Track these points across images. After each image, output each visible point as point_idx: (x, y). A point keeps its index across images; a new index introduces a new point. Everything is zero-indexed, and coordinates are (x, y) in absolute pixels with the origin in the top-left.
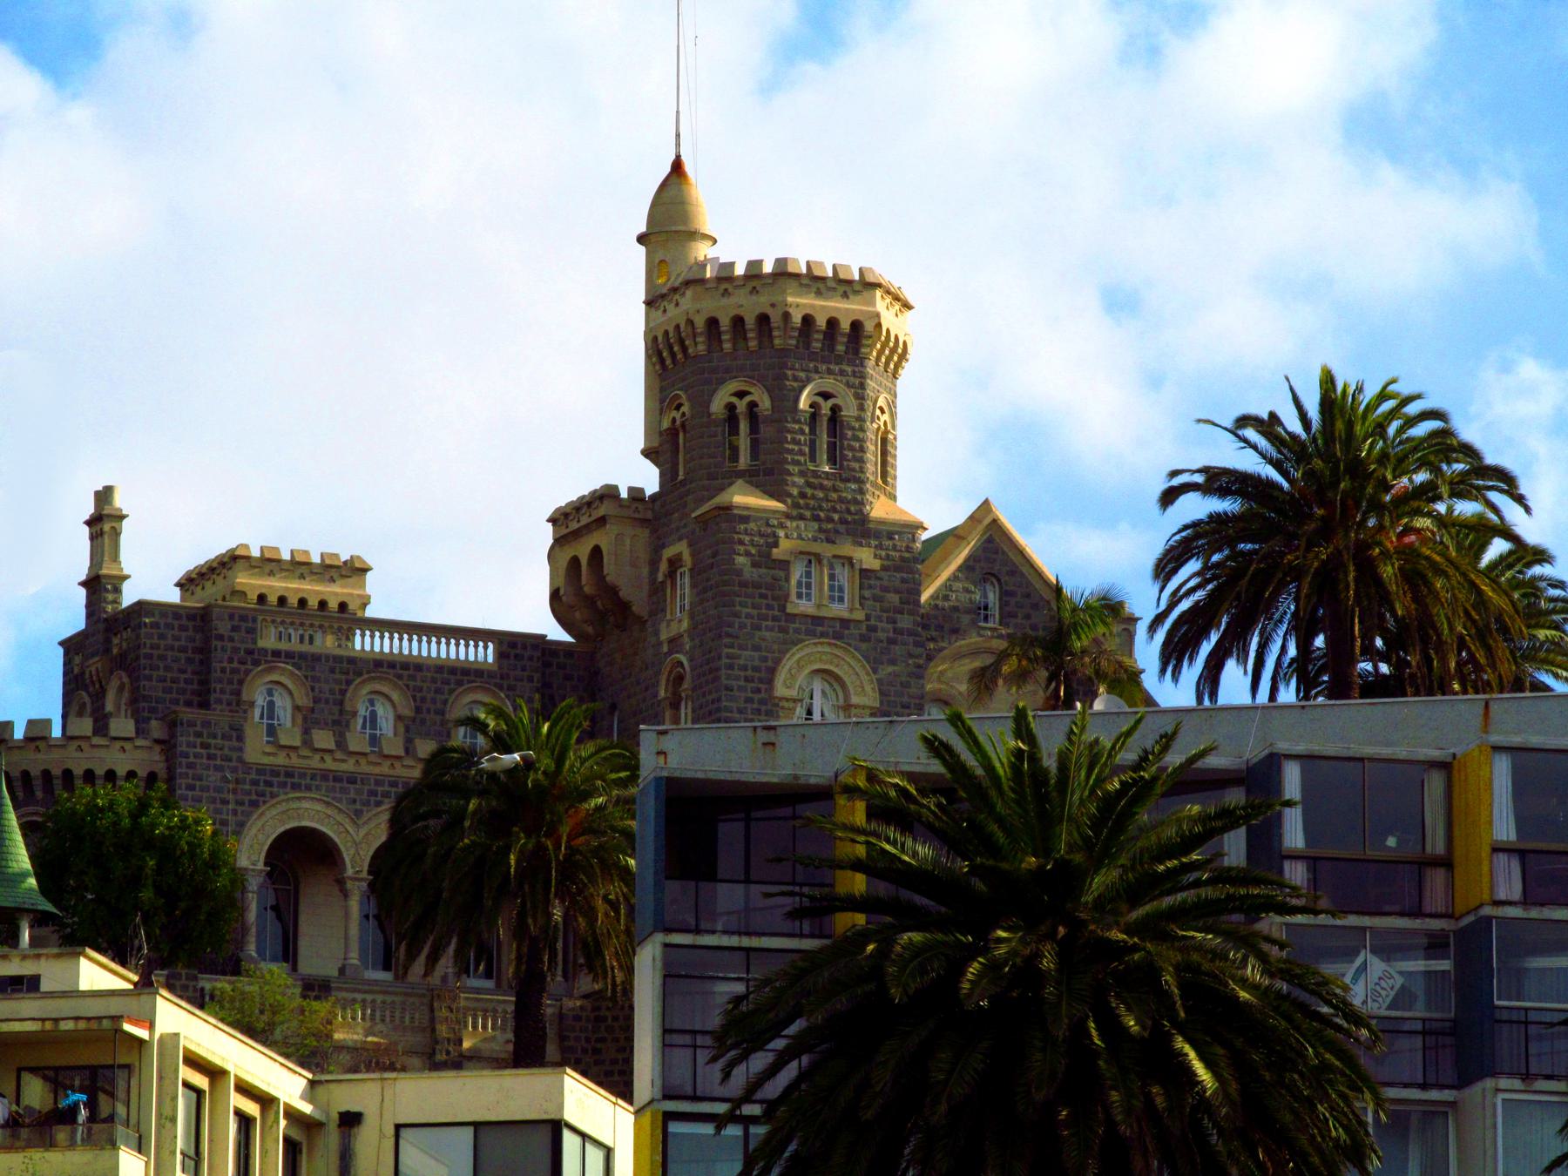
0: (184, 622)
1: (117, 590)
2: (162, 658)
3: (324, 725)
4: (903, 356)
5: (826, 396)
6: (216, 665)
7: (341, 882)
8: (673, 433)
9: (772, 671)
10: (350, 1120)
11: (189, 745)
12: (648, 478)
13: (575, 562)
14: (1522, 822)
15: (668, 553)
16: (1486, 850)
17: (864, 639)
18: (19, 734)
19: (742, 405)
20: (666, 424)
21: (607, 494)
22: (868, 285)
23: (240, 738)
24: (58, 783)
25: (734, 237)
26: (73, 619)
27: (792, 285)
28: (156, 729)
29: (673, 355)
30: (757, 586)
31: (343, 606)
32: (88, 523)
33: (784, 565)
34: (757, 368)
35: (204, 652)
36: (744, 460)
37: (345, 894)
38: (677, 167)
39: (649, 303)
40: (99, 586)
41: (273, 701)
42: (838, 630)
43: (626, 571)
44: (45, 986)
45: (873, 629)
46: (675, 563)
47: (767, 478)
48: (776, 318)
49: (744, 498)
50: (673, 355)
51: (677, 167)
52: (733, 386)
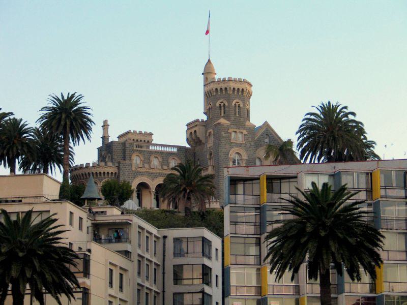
0: (121, 145)
1: (108, 139)
2: (117, 151)
3: (165, 165)
4: (251, 95)
5: (237, 102)
6: (126, 152)
7: (150, 192)
8: (209, 109)
9: (228, 153)
10: (165, 237)
11: (123, 167)
12: (205, 118)
13: (191, 133)
14: (385, 183)
15: (209, 131)
16: (379, 187)
17: (245, 147)
18: (91, 165)
19: (222, 104)
20: (208, 108)
21: (197, 121)
22: (245, 82)
23: (131, 166)
24: (98, 174)
25: (221, 73)
26: (100, 144)
27: (231, 82)
28: (117, 165)
29: (209, 95)
30: (225, 137)
31: (148, 141)
32: (102, 127)
33: (231, 133)
34: (225, 100)
35: (124, 151)
36: (222, 115)
37: (151, 194)
38: (209, 61)
39: (204, 86)
40: (104, 138)
41: (136, 160)
42: (240, 145)
43: (201, 134)
44: (108, 214)
45: (246, 145)
46: (210, 133)
47: (227, 117)
48: (228, 88)
49: (223, 121)
50: (209, 95)
51: (209, 61)
52: (221, 101)
